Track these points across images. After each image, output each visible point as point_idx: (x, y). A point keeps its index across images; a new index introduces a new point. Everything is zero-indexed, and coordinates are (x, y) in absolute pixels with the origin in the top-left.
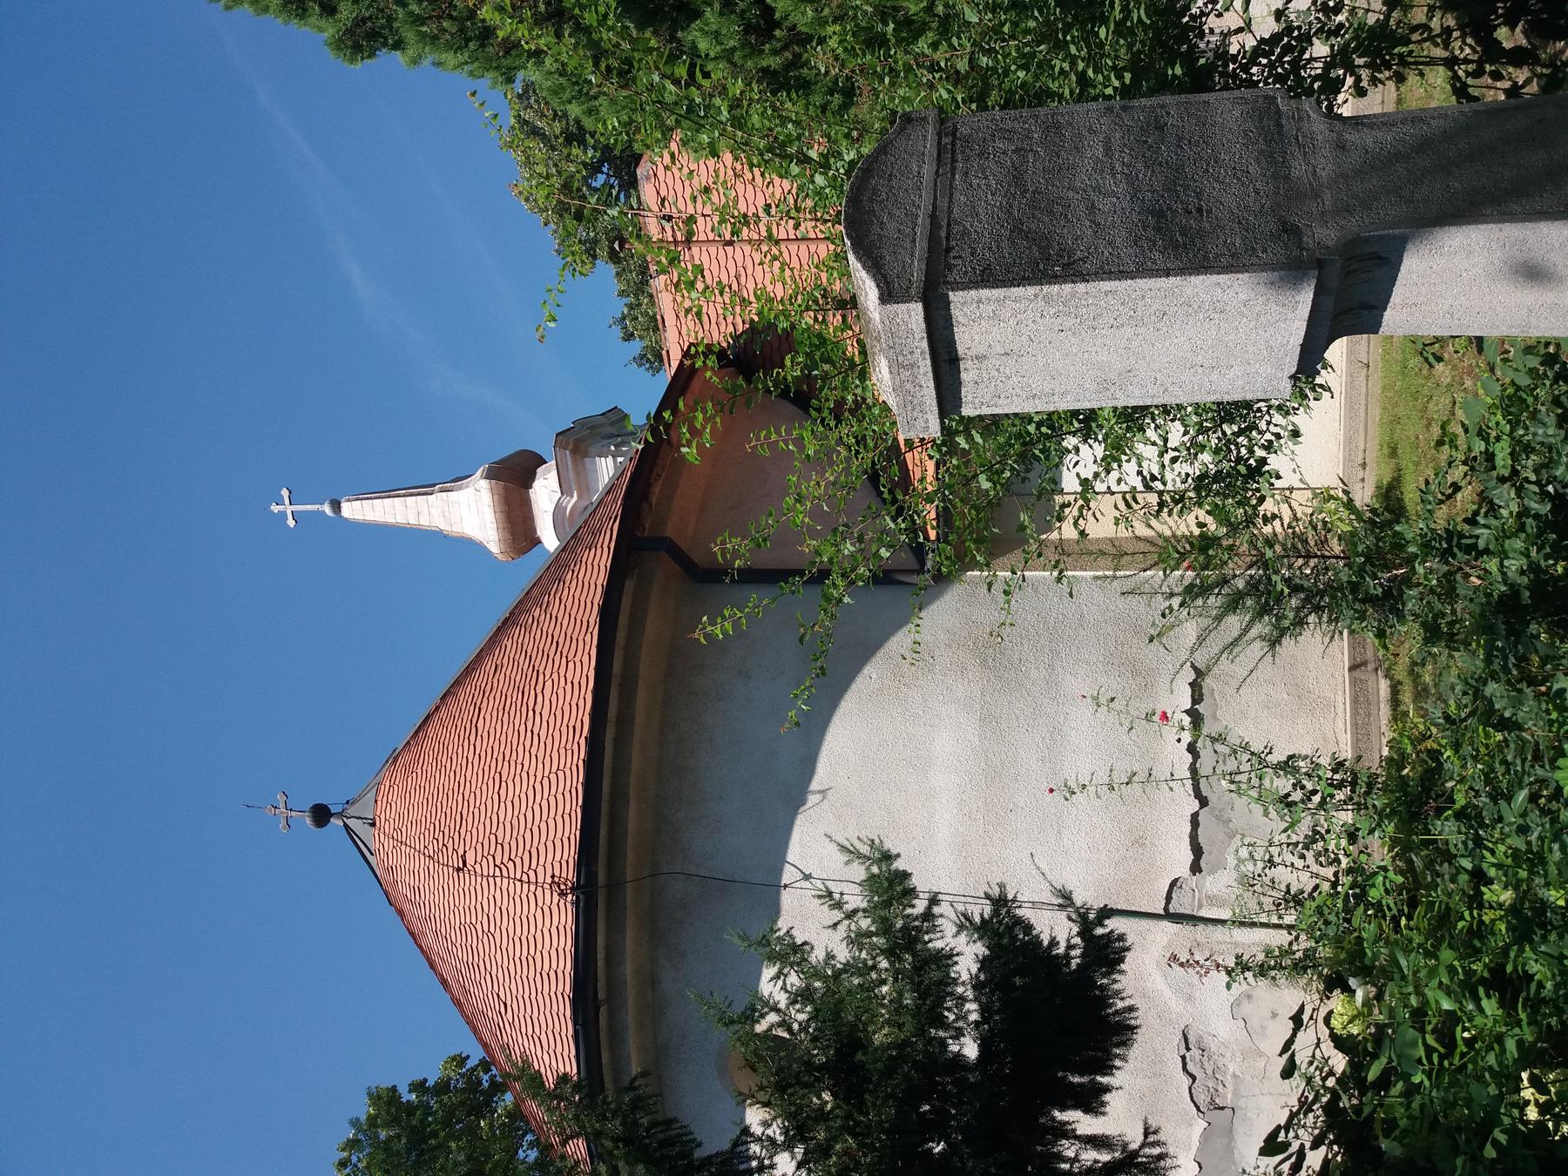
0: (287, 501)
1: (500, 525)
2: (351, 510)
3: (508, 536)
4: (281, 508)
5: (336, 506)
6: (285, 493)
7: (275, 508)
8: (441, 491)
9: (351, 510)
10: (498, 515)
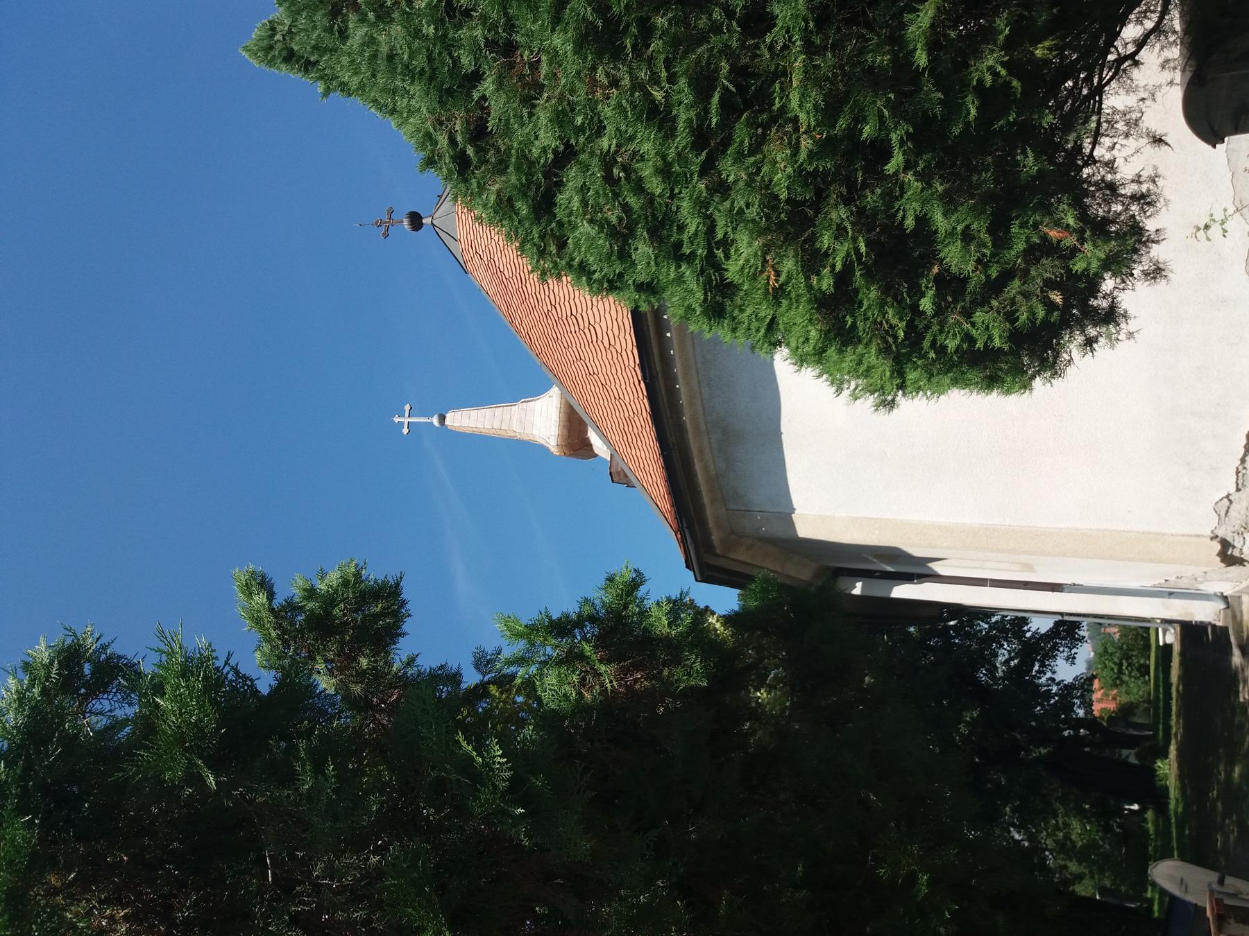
0: (407, 415)
1: (561, 424)
2: (459, 420)
3: (565, 432)
4: (401, 419)
5: (442, 418)
6: (407, 408)
7: (397, 420)
8: (523, 402)
9: (459, 420)
10: (562, 415)
